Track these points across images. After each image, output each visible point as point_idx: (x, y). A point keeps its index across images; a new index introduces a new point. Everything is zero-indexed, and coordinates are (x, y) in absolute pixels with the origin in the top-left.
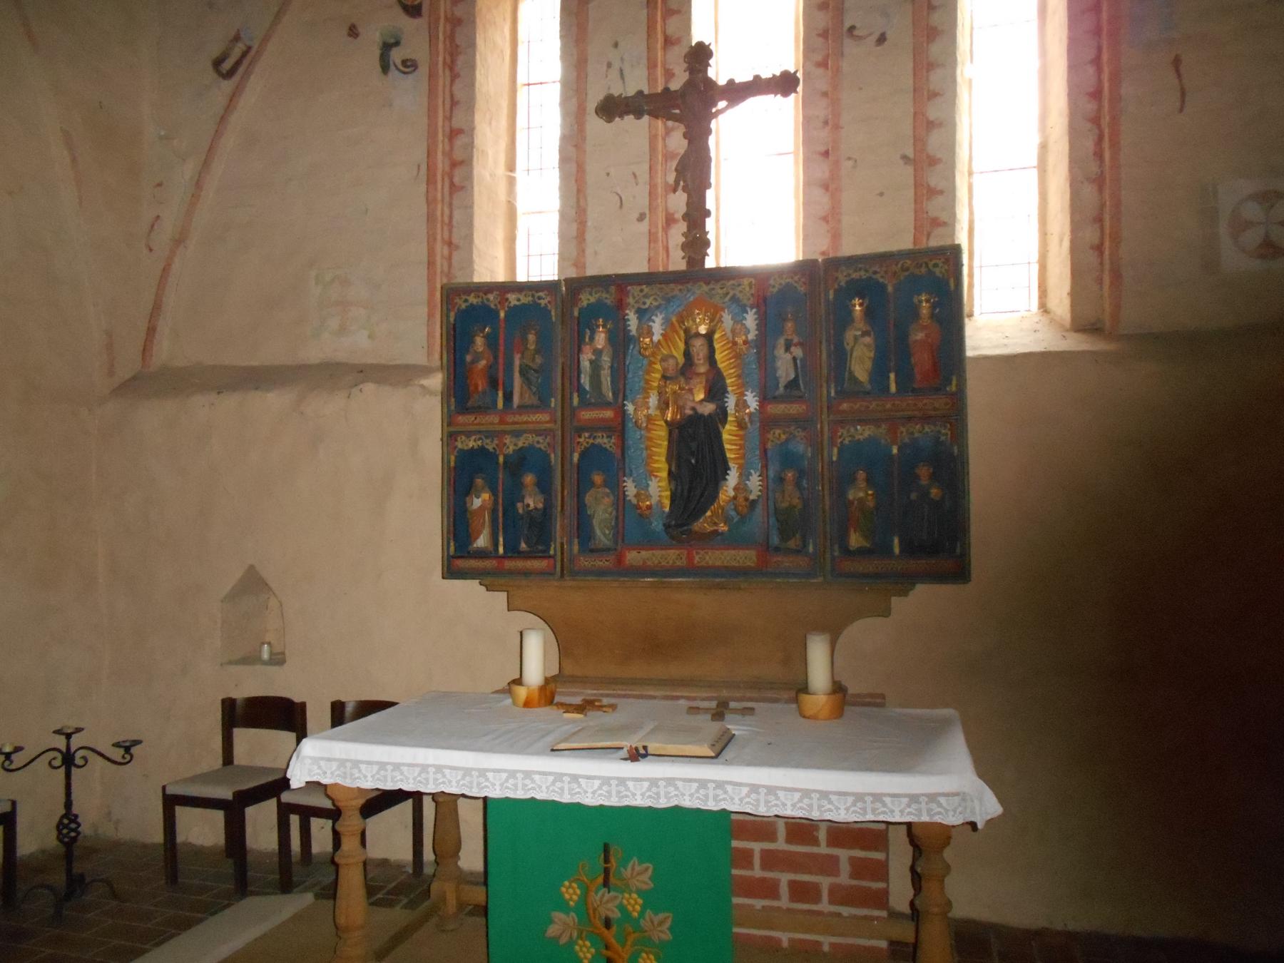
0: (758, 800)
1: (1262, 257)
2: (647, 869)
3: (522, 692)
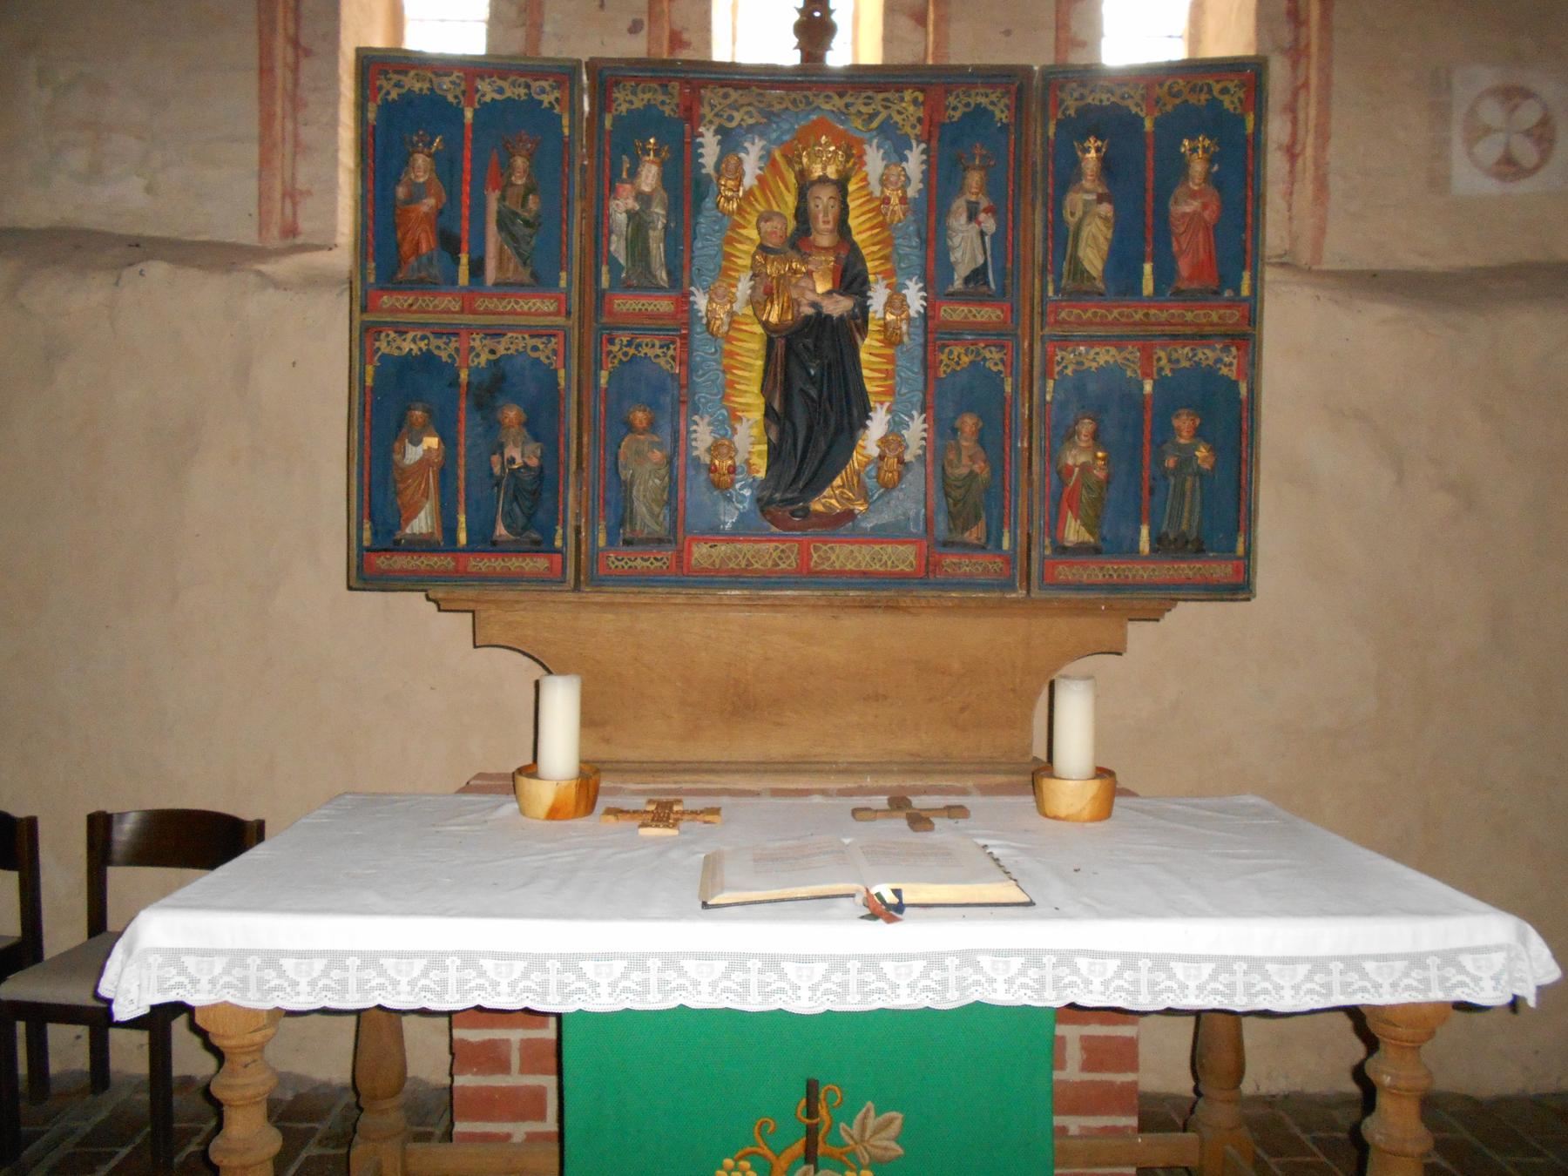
0: (1136, 982)
1: (1501, 177)
2: (891, 1121)
3: (543, 793)
